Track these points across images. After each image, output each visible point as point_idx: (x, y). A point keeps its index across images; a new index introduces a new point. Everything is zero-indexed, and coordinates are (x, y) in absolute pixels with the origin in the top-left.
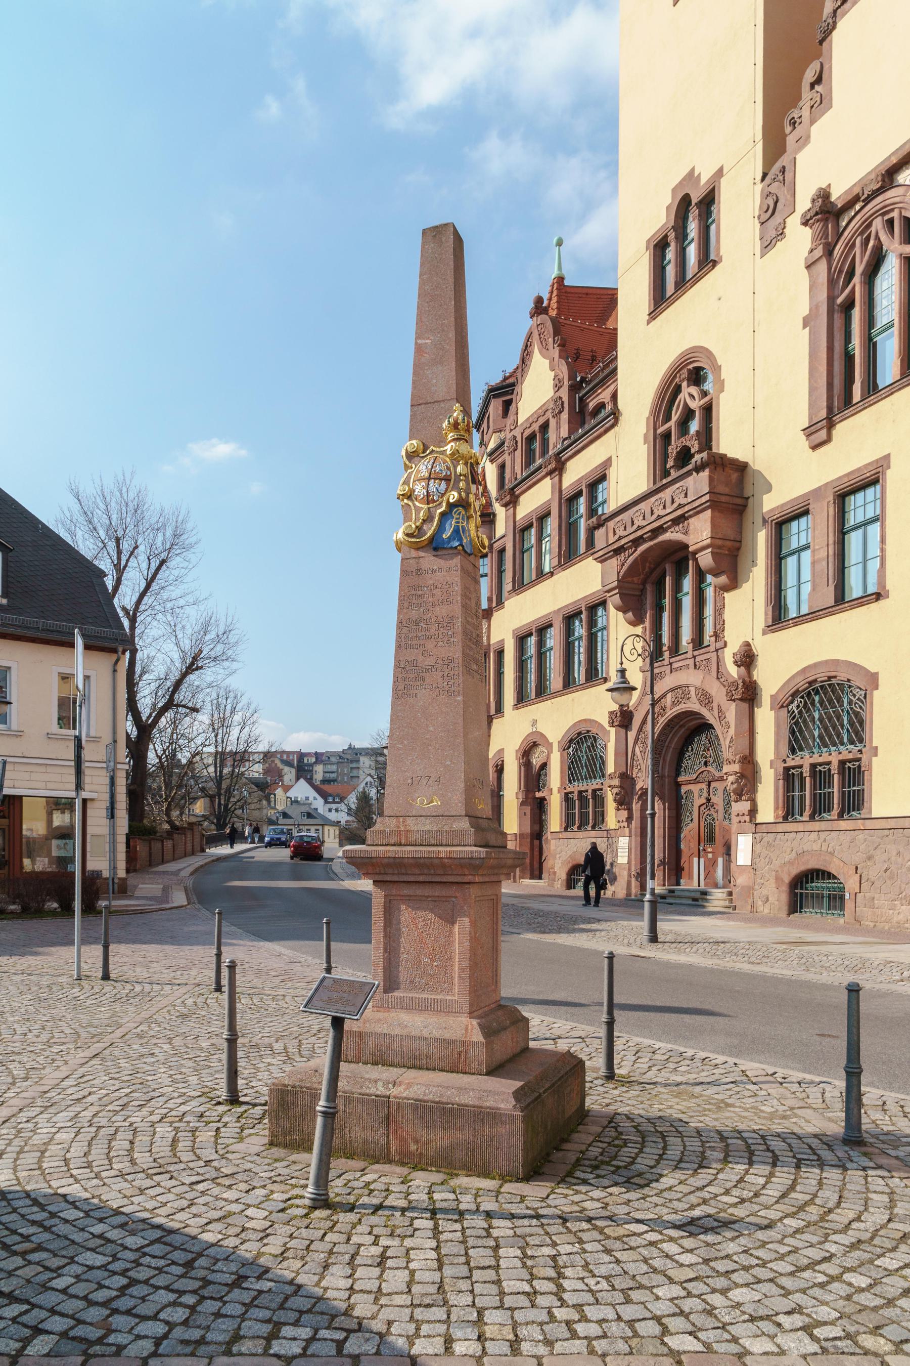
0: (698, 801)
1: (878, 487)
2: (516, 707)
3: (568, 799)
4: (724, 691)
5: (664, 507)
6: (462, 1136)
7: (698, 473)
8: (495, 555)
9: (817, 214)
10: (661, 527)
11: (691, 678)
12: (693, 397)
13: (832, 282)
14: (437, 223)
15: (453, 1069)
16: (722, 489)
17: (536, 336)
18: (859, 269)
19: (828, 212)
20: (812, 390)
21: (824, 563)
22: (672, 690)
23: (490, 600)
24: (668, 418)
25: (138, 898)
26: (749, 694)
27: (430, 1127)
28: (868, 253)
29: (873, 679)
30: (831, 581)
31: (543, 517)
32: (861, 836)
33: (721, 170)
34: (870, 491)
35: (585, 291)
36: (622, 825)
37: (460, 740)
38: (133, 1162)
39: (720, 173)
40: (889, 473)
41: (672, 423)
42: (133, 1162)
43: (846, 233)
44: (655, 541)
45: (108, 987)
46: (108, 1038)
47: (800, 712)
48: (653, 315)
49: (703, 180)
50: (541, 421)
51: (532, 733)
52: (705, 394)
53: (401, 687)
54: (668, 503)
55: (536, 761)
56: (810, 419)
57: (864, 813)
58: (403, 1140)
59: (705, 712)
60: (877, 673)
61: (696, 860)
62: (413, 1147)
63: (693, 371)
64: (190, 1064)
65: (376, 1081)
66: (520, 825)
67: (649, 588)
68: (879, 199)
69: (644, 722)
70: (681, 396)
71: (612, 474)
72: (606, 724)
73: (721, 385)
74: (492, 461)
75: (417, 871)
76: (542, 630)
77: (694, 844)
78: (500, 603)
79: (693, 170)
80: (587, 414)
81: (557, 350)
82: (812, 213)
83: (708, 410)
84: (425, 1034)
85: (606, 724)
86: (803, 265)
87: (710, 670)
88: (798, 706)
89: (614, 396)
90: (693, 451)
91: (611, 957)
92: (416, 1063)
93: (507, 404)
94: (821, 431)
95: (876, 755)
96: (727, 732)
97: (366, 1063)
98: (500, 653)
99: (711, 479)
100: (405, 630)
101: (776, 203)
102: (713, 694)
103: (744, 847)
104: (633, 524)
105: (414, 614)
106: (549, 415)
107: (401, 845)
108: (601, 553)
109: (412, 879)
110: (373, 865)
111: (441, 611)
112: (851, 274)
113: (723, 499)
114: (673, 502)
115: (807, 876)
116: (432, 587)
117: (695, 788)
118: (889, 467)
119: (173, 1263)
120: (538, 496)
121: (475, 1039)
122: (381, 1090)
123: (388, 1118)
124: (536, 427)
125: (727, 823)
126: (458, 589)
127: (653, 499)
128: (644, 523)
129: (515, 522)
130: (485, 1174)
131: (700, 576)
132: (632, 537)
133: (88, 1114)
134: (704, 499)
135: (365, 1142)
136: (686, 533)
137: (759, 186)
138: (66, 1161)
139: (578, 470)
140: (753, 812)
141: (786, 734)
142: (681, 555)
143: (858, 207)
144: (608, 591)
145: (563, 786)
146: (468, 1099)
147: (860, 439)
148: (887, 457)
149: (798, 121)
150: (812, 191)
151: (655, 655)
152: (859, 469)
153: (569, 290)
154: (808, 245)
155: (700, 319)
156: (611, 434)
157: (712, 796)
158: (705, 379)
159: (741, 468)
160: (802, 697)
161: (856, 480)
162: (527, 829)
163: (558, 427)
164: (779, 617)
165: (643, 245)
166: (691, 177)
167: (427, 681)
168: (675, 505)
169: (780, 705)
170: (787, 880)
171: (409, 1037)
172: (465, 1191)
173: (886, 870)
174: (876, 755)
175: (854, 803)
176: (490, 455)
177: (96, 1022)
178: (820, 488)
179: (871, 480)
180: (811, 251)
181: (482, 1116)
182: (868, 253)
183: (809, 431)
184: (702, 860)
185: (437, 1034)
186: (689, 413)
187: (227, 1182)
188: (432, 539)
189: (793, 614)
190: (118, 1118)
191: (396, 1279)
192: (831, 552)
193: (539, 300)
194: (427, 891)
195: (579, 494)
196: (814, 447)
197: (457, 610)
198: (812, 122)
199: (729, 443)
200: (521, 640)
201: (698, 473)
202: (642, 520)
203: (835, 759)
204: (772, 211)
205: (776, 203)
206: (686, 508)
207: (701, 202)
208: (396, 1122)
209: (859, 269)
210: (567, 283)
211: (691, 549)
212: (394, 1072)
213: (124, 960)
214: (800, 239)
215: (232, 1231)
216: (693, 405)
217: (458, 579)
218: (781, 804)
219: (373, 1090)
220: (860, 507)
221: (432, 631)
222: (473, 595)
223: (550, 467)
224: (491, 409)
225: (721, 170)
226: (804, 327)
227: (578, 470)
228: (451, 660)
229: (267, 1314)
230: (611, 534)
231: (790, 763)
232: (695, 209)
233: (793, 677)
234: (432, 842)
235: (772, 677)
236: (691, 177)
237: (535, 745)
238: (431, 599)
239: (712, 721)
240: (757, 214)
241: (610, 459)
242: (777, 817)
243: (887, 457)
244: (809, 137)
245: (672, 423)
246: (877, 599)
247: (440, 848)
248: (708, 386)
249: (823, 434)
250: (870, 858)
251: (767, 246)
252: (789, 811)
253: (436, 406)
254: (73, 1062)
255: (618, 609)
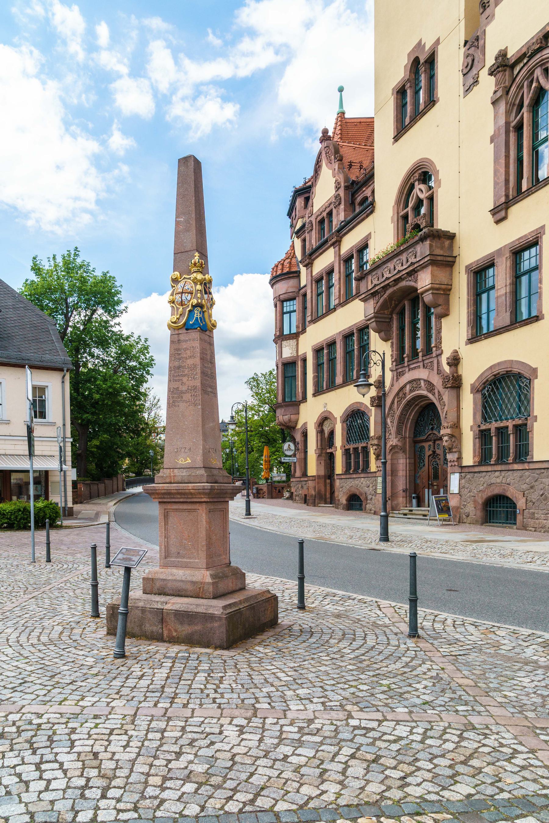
0: (428, 453)
1: (538, 247)
2: (314, 395)
3: (347, 453)
4: (441, 381)
5: (402, 265)
6: (198, 627)
7: (422, 242)
8: (301, 298)
9: (498, 67)
10: (400, 278)
11: (422, 374)
12: (422, 191)
13: (508, 113)
14: (185, 155)
15: (197, 597)
16: (438, 252)
17: (324, 155)
18: (526, 102)
19: (506, 66)
20: (496, 184)
21: (504, 298)
22: (410, 382)
23: (297, 327)
24: (406, 206)
25: (80, 519)
26: (455, 383)
27: (182, 623)
28: (532, 91)
29: (535, 371)
30: (508, 309)
31: (330, 272)
32: (527, 473)
33: (438, 40)
34: (533, 250)
35: (359, 121)
36: (380, 469)
37: (200, 428)
38: (39, 640)
39: (438, 42)
40: (544, 237)
41: (409, 209)
42: (39, 640)
43: (517, 79)
44: (397, 287)
45: (49, 566)
46: (43, 590)
47: (489, 394)
48: (397, 138)
49: (427, 48)
50: (328, 210)
51: (324, 411)
52: (430, 188)
53: (171, 402)
54: (404, 263)
55: (327, 430)
56: (495, 204)
57: (529, 459)
58: (169, 630)
59: (430, 396)
60: (537, 368)
61: (426, 490)
62: (174, 634)
63: (423, 174)
64: (81, 601)
65: (157, 602)
66: (317, 470)
67: (395, 317)
68: (538, 56)
69: (393, 403)
70: (414, 191)
71: (371, 243)
72: (369, 405)
73: (438, 182)
74: (298, 237)
75: (179, 496)
76: (331, 344)
77: (425, 480)
78: (304, 330)
79: (421, 40)
80: (356, 204)
81: (337, 163)
82: (495, 67)
83: (431, 199)
84: (183, 579)
85: (369, 405)
86: (489, 102)
87: (433, 370)
88: (488, 391)
89: (373, 192)
90: (422, 227)
91: (413, 557)
92: (179, 594)
93: (307, 200)
94: (500, 212)
95: (536, 421)
96: (445, 410)
97: (155, 594)
98: (304, 360)
99: (431, 246)
100: (173, 372)
101: (473, 60)
102: (435, 384)
103: (454, 482)
104: (383, 276)
105: (177, 364)
106: (332, 206)
107: (171, 483)
108: (363, 296)
109: (177, 500)
110: (158, 494)
111: (190, 362)
112: (521, 106)
113: (439, 258)
114: (407, 261)
115: (493, 499)
116: (186, 349)
117: (426, 445)
118: (544, 234)
119: (46, 676)
120: (325, 260)
121: (207, 581)
122: (160, 606)
123: (162, 619)
124: (325, 214)
125: (445, 466)
126: (198, 350)
127: (395, 260)
128: (390, 275)
129: (312, 276)
130: (207, 646)
131: (427, 309)
132: (382, 285)
133: (23, 622)
134: (426, 259)
135: (152, 632)
136: (416, 281)
137: (463, 50)
138: (8, 640)
139: (350, 242)
140: (460, 458)
141: (480, 407)
142: (414, 295)
143: (525, 61)
144: (369, 320)
145: (343, 446)
146: (201, 610)
147: (525, 218)
148: (543, 227)
149: (487, 5)
150: (496, 53)
151: (399, 360)
152: (525, 236)
153: (348, 121)
154: (493, 89)
155: (426, 140)
156: (371, 217)
157: (437, 450)
158: (430, 179)
159: (451, 237)
160: (491, 385)
161: (523, 242)
162: (322, 473)
163: (338, 214)
164: (477, 334)
165: (391, 92)
166: (420, 45)
167: (184, 398)
168: (409, 263)
169: (475, 390)
170: (480, 501)
171: (175, 580)
172: (194, 653)
173: (542, 495)
174: (536, 421)
175: (523, 452)
176: (297, 233)
177: (37, 583)
178: (501, 248)
179: (533, 242)
180: (495, 92)
181: (208, 618)
182: (532, 91)
183: (494, 212)
184: (430, 490)
185: (189, 578)
186: (419, 203)
187: (81, 648)
188: (185, 324)
189: (485, 331)
190: (38, 623)
191: (144, 683)
192: (508, 291)
193: (325, 132)
194: (185, 507)
195: (352, 257)
196: (497, 222)
197: (197, 361)
198: (496, 5)
199: (443, 222)
200: (318, 351)
201: (422, 242)
202: (388, 273)
203: (510, 424)
204: (470, 67)
205: (473, 60)
206: (416, 266)
207: (426, 62)
208: (166, 622)
209: (526, 102)
210: (347, 116)
211: (419, 291)
212: (168, 598)
213: (61, 552)
214: (488, 84)
215: (77, 666)
216: (422, 196)
217: (198, 345)
218: (477, 454)
219: (156, 606)
220: (528, 260)
221: (186, 372)
222: (209, 352)
223: (333, 240)
224: (297, 203)
225: (438, 40)
226: (491, 142)
227: (350, 242)
228: (195, 388)
229: (81, 693)
230: (370, 283)
231: (483, 427)
232: (423, 66)
233: (485, 372)
234: (186, 481)
235: (472, 372)
236: (420, 45)
237: (326, 419)
238: (185, 356)
239: (435, 401)
240: (461, 69)
241: (370, 234)
242: (475, 462)
243: (543, 227)
244: (494, 15)
245: (409, 209)
246: (537, 320)
247: (189, 485)
248: (432, 184)
249: (503, 214)
250: (532, 487)
251: (468, 91)
252: (484, 457)
253: (186, 254)
254: (20, 600)
255: (375, 331)
